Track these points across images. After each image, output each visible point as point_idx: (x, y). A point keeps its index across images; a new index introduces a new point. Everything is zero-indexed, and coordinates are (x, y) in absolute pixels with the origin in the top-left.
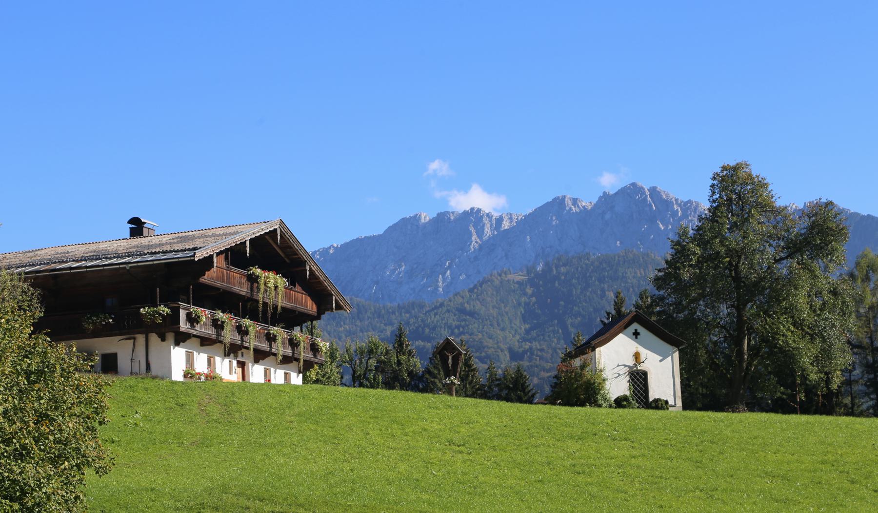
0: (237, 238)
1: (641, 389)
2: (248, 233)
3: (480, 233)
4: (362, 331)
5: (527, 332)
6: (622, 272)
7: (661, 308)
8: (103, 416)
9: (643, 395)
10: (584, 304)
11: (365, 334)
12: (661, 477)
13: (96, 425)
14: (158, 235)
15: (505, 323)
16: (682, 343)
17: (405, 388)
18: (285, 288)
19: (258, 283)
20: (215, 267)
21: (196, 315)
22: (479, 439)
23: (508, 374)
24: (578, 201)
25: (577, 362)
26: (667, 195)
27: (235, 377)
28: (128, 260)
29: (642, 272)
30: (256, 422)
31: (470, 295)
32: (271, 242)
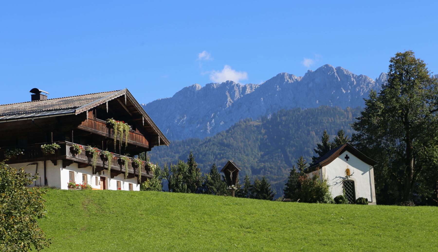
0: (101, 100)
1: (351, 192)
2: (107, 98)
3: (232, 97)
4: (160, 157)
5: (262, 156)
6: (320, 119)
7: (359, 142)
8: (40, 213)
9: (352, 195)
10: (297, 139)
11: (162, 159)
12: (376, 247)
13: (36, 218)
14: (50, 99)
15: (249, 151)
16: (376, 163)
17: (194, 192)
18: (130, 131)
19: (113, 128)
20: (87, 119)
21: (76, 149)
22: (259, 224)
23: (257, 183)
24: (292, 76)
25: (311, 175)
26: (347, 72)
27: (99, 187)
28: (33, 115)
29: (332, 119)
30: (120, 215)
31: (226, 134)
32: (120, 103)
